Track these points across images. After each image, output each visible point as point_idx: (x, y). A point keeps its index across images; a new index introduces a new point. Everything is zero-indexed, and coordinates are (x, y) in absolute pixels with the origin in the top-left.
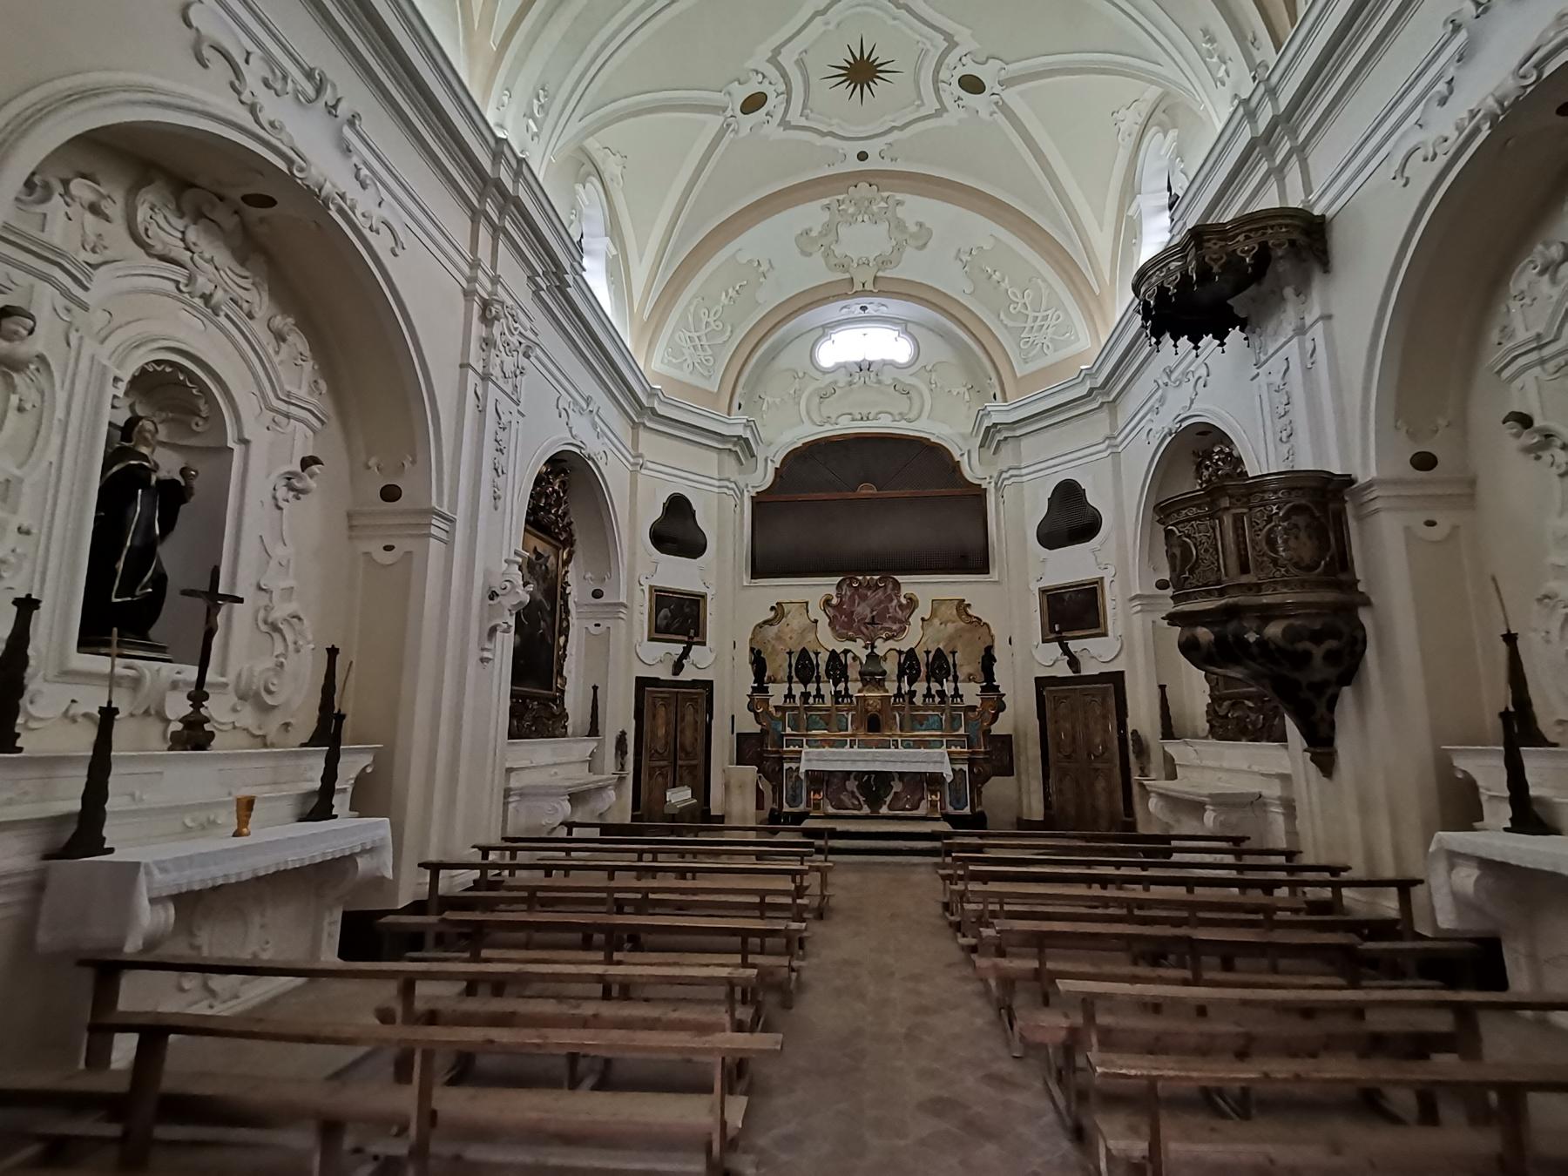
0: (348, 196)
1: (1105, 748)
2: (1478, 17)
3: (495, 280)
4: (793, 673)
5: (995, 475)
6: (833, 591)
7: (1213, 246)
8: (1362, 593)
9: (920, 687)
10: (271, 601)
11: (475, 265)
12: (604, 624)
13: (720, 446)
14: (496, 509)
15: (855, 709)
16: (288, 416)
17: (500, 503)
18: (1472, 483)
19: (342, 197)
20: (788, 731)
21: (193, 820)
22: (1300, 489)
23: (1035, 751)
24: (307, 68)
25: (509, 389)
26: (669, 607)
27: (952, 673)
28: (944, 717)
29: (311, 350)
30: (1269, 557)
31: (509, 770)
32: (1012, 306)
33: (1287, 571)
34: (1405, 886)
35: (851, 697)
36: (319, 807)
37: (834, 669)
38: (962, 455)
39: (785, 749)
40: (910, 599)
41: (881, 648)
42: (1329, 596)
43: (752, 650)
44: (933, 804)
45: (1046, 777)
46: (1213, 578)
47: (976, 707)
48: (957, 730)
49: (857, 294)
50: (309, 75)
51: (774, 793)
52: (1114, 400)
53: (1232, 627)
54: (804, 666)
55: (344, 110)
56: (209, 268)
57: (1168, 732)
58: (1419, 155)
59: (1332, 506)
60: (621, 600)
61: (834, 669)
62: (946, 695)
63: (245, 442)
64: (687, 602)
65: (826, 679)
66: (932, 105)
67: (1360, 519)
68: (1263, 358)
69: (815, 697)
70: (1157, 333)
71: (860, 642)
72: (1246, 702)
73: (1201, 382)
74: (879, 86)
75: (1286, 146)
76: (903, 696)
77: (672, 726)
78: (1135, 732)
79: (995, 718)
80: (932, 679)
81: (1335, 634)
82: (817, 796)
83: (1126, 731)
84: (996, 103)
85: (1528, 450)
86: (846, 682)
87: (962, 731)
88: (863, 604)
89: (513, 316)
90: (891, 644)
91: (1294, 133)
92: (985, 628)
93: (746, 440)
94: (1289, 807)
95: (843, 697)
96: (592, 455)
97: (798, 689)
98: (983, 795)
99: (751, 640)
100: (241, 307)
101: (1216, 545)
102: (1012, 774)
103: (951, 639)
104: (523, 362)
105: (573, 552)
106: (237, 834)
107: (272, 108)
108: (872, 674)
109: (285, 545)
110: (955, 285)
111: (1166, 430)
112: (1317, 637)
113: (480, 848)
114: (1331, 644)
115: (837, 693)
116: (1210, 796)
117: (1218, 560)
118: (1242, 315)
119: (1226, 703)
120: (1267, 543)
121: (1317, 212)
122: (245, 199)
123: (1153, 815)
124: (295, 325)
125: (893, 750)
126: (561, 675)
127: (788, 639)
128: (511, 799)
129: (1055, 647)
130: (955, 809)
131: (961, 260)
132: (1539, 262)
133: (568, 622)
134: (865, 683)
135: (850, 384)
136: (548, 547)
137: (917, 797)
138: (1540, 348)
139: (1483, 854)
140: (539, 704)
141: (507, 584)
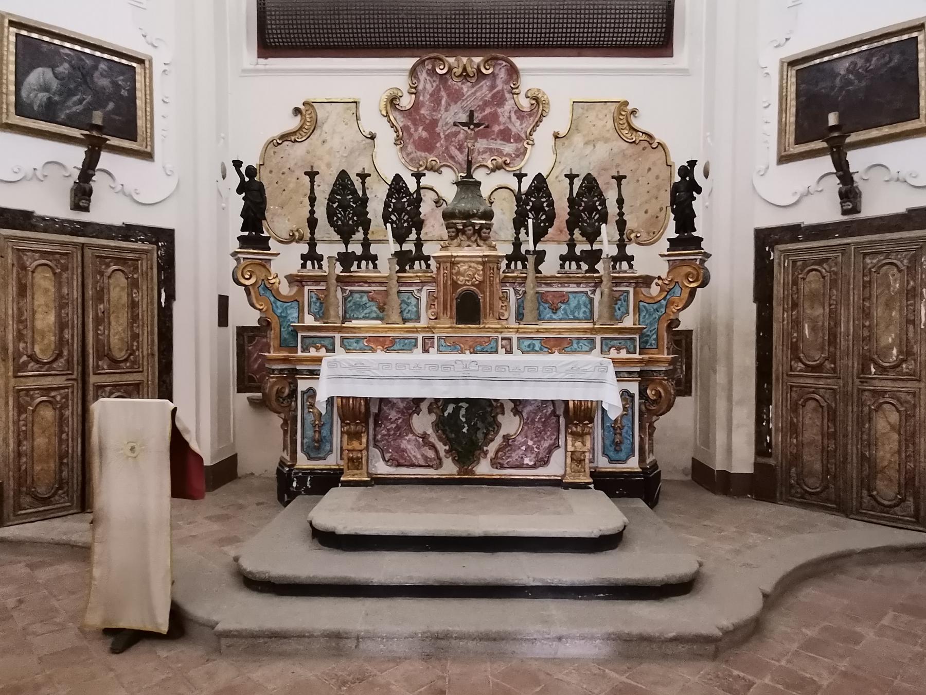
6: (402, 83)
15: (434, 280)
20: (309, 320)
28: (597, 297)
39: (300, 354)
40: (536, 99)
45: (763, 400)
54: (344, 206)
82: (355, 444)
88: (454, 108)
108: (467, 215)
130: (611, 461)
134: (456, 233)
137: (546, 444)
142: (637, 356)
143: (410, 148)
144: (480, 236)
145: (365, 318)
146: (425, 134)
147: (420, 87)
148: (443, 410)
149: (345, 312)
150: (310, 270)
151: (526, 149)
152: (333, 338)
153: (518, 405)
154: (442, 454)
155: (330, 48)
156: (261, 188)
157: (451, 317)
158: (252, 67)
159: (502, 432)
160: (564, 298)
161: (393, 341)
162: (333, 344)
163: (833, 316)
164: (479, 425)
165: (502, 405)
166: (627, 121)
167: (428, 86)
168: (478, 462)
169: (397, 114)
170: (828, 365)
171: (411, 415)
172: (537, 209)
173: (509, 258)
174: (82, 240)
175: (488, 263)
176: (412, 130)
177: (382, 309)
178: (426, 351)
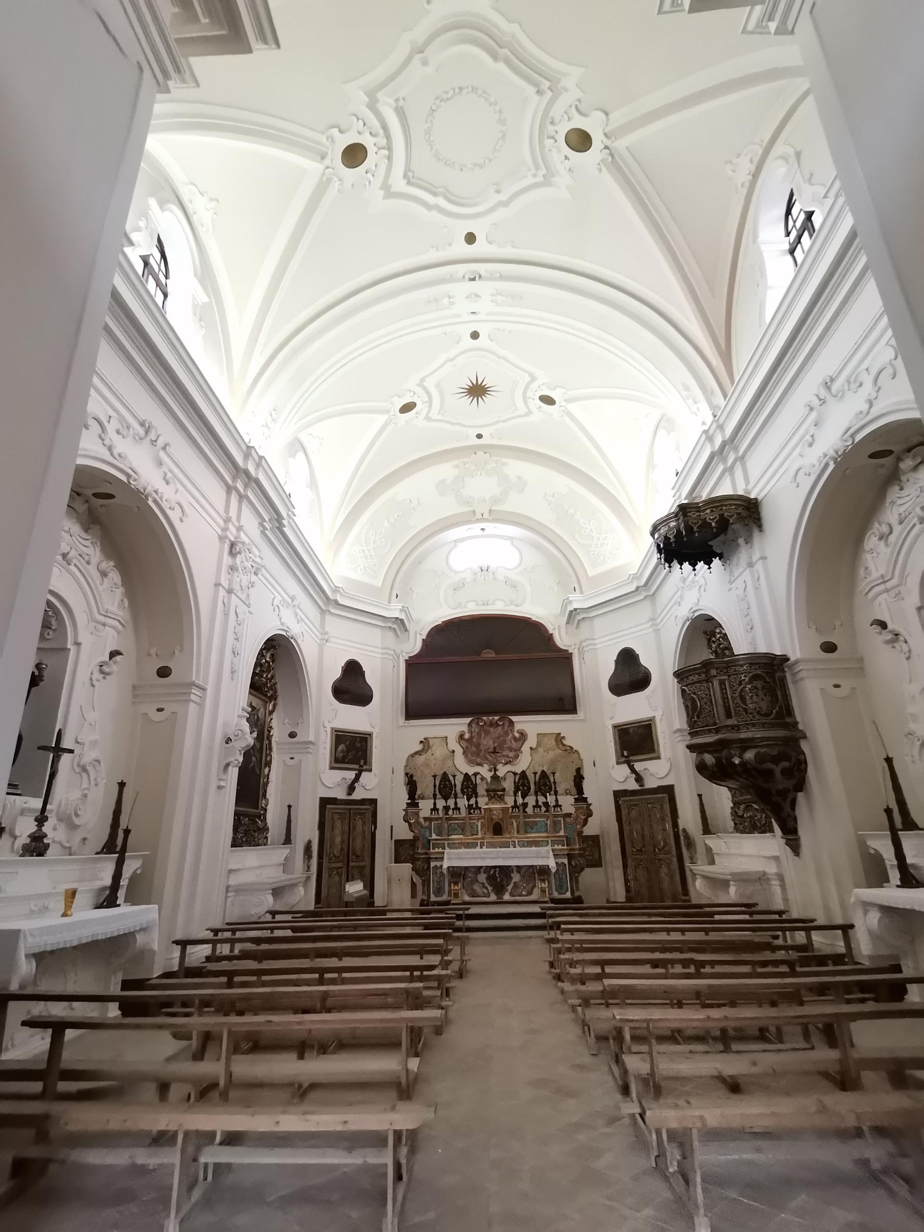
0: (160, 491)
1: (666, 844)
2: (821, 405)
3: (240, 529)
4: (437, 792)
5: (578, 643)
6: (465, 729)
7: (693, 515)
8: (801, 731)
9: (531, 800)
10: (83, 750)
11: (227, 520)
12: (297, 757)
13: (383, 625)
14: (232, 680)
15: (484, 818)
16: (104, 625)
17: (235, 675)
18: (861, 660)
19: (156, 492)
20: (434, 836)
21: (36, 905)
22: (757, 664)
23: (616, 847)
24: (141, 420)
25: (243, 597)
27: (553, 789)
29: (122, 581)
31: (230, 871)
32: (582, 530)
33: (753, 717)
34: (846, 929)
35: (480, 808)
36: (109, 900)
37: (468, 787)
38: (554, 629)
40: (521, 733)
41: (502, 770)
42: (780, 733)
43: (407, 774)
44: (543, 891)
45: (625, 866)
46: (711, 722)
47: (572, 814)
48: (559, 832)
49: (478, 521)
50: (142, 424)
51: (424, 886)
52: (654, 594)
53: (725, 753)
54: (445, 786)
55: (160, 443)
56: (66, 536)
58: (801, 473)
59: (778, 674)
60: (310, 739)
61: (468, 787)
63: (78, 644)
64: (358, 739)
65: (462, 796)
66: (522, 409)
67: (795, 682)
68: (733, 579)
69: (453, 809)
70: (669, 560)
71: (486, 767)
72: (754, 805)
73: (702, 589)
74: (487, 398)
75: (731, 458)
77: (346, 837)
78: (684, 830)
79: (585, 822)
80: (539, 793)
81: (788, 759)
82: (456, 887)
84: (564, 411)
85: (888, 642)
86: (476, 797)
87: (562, 833)
89: (249, 550)
90: (508, 768)
91: (736, 449)
92: (575, 755)
93: (402, 621)
94: (781, 878)
95: (474, 809)
96: (294, 636)
97: (441, 803)
100: (83, 559)
101: (711, 700)
102: (601, 866)
103: (553, 762)
104: (254, 578)
105: (277, 704)
106: (64, 915)
107: (122, 445)
108: (495, 791)
109: (94, 710)
110: (544, 516)
111: (686, 618)
112: (776, 760)
113: (212, 930)
114: (785, 764)
116: (732, 874)
117: (713, 709)
118: (719, 551)
119: (742, 807)
120: (740, 698)
121: (752, 496)
122: (94, 495)
123: (699, 890)
124: (114, 566)
125: (512, 849)
126: (265, 798)
127: (432, 765)
128: (229, 894)
129: (625, 769)
130: (559, 894)
131: (547, 500)
132: (877, 534)
134: (491, 798)
135: (475, 580)
136: (259, 702)
137: (531, 885)
138: (884, 582)
139: (879, 902)
140: (249, 820)
141: (239, 732)
142: (565, 847)
143: (469, 755)
147: (473, 730)
152: (444, 843)
153: (519, 868)
154: (490, 891)
159: (513, 881)
160: (536, 823)
163: (642, 828)
165: (512, 869)
169: (463, 742)
170: (644, 849)
171: (477, 875)
172: (523, 785)
173: (513, 807)
175: (505, 810)
177: (463, 830)
178: (481, 848)
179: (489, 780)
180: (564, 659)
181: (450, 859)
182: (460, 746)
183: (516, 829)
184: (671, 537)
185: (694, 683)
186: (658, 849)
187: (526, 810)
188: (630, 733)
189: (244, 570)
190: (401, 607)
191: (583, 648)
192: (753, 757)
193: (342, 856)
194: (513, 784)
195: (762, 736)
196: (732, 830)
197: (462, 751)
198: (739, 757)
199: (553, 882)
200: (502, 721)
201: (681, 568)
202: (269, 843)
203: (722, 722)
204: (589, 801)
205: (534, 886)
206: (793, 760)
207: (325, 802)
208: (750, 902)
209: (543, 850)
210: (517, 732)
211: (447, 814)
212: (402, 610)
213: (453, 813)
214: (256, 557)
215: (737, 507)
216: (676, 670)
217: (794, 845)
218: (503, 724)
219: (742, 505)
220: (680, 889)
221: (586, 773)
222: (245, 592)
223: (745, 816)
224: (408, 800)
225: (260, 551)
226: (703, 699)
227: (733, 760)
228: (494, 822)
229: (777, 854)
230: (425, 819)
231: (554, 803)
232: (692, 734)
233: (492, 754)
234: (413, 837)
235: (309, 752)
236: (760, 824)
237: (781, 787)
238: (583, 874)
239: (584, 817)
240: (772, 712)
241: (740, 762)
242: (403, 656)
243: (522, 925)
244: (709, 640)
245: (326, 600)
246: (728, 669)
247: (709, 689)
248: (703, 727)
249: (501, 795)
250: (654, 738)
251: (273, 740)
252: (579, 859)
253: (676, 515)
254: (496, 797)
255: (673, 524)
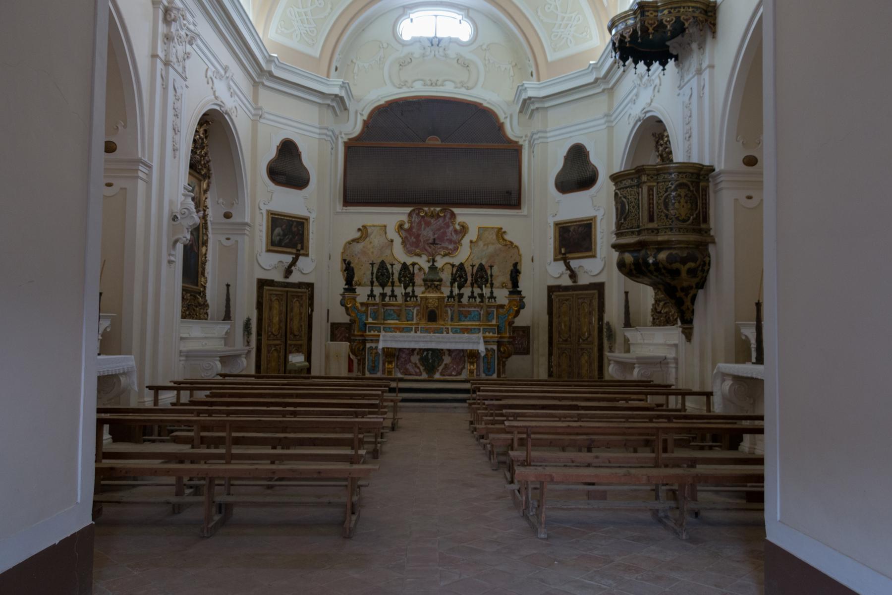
1: (590, 335)
4: (375, 279)
5: (529, 135)
6: (405, 218)
8: (712, 236)
9: (466, 291)
14: (175, 158)
15: (419, 305)
17: (177, 153)
20: (370, 320)
22: (684, 173)
25: (180, 70)
26: (281, 227)
27: (489, 282)
28: (482, 313)
30: (664, 213)
31: (182, 339)
33: (672, 222)
34: (709, 395)
38: (506, 118)
39: (367, 333)
41: (440, 262)
42: (692, 237)
43: (344, 260)
44: (471, 372)
45: (550, 354)
47: (505, 305)
48: (491, 321)
51: (359, 364)
52: (612, 88)
53: (643, 252)
54: (382, 275)
57: (628, 324)
59: (701, 184)
61: (405, 276)
62: (484, 297)
64: (295, 223)
65: (398, 284)
67: (716, 192)
68: (682, 84)
69: (390, 296)
70: (624, 59)
76: (454, 297)
78: (608, 323)
79: (517, 313)
81: (694, 260)
82: (390, 366)
83: (602, 324)
86: (413, 285)
87: (494, 322)
88: (427, 229)
89: (183, 16)
90: (447, 259)
93: (342, 98)
94: (676, 360)
97: (378, 291)
98: (506, 367)
99: (343, 253)
101: (639, 204)
104: (189, 48)
108: (432, 281)
111: (637, 118)
112: (684, 261)
114: (691, 265)
115: (407, 295)
116: (637, 358)
117: (639, 213)
118: (675, 53)
120: (664, 204)
123: (612, 371)
126: (204, 276)
129: (560, 267)
130: (487, 375)
133: (207, 236)
135: (424, 55)
137: (460, 367)
140: (191, 295)
141: (186, 211)
143: (408, 246)
144: (437, 288)
145: (392, 320)
146: (414, 240)
148: (422, 354)
149: (384, 317)
150: (371, 301)
151: (458, 247)
152: (380, 327)
153: (450, 351)
154: (422, 370)
155: (376, 203)
156: (353, 270)
157: (426, 320)
158: (340, 211)
161: (403, 328)
162: (380, 329)
164: (436, 359)
166: (502, 237)
167: (416, 220)
168: (435, 373)
169: (403, 232)
170: (569, 339)
172: (461, 277)
173: (449, 297)
174: (287, 289)
176: (409, 238)
177: (399, 316)
179: (427, 270)
180: (514, 151)
181: (385, 341)
182: (399, 236)
183: (450, 316)
184: (627, 36)
185: (626, 188)
186: (582, 339)
187: (462, 300)
188: (570, 231)
189: (180, 40)
190: (341, 83)
191: (534, 141)
192: (665, 259)
193: (280, 334)
194: (450, 275)
195: (676, 239)
196: (651, 324)
197: (400, 240)
198: (654, 258)
199: (482, 365)
200: (444, 212)
201: (635, 68)
202: (209, 319)
203: (644, 225)
204: (523, 294)
205: (464, 368)
206: (698, 263)
207: (262, 284)
208: (649, 380)
209: (474, 336)
210: (459, 225)
211: (383, 300)
212: (343, 86)
213: (390, 299)
214: (189, 24)
215: (695, 10)
216: (622, 170)
217: (688, 334)
218: (445, 216)
219: (699, 8)
220: (596, 373)
221: (525, 268)
222: (181, 64)
223: (662, 311)
224: (346, 285)
225: (193, 17)
226: (631, 202)
227: (648, 259)
228: (429, 309)
229: (676, 342)
230: (362, 304)
231: (489, 295)
232: (619, 235)
233: (432, 246)
234: (350, 320)
235: (245, 234)
236: (673, 318)
237: (685, 284)
238: (509, 359)
239: (516, 309)
240: (689, 218)
241: (653, 261)
242: (342, 138)
243: (449, 398)
244: (657, 142)
245: (259, 71)
246: (659, 176)
247: (638, 194)
248: (627, 229)
249: (438, 285)
250: (593, 237)
251: (208, 219)
252: (508, 346)
253: (635, 13)
254: (433, 286)
255: (631, 22)
